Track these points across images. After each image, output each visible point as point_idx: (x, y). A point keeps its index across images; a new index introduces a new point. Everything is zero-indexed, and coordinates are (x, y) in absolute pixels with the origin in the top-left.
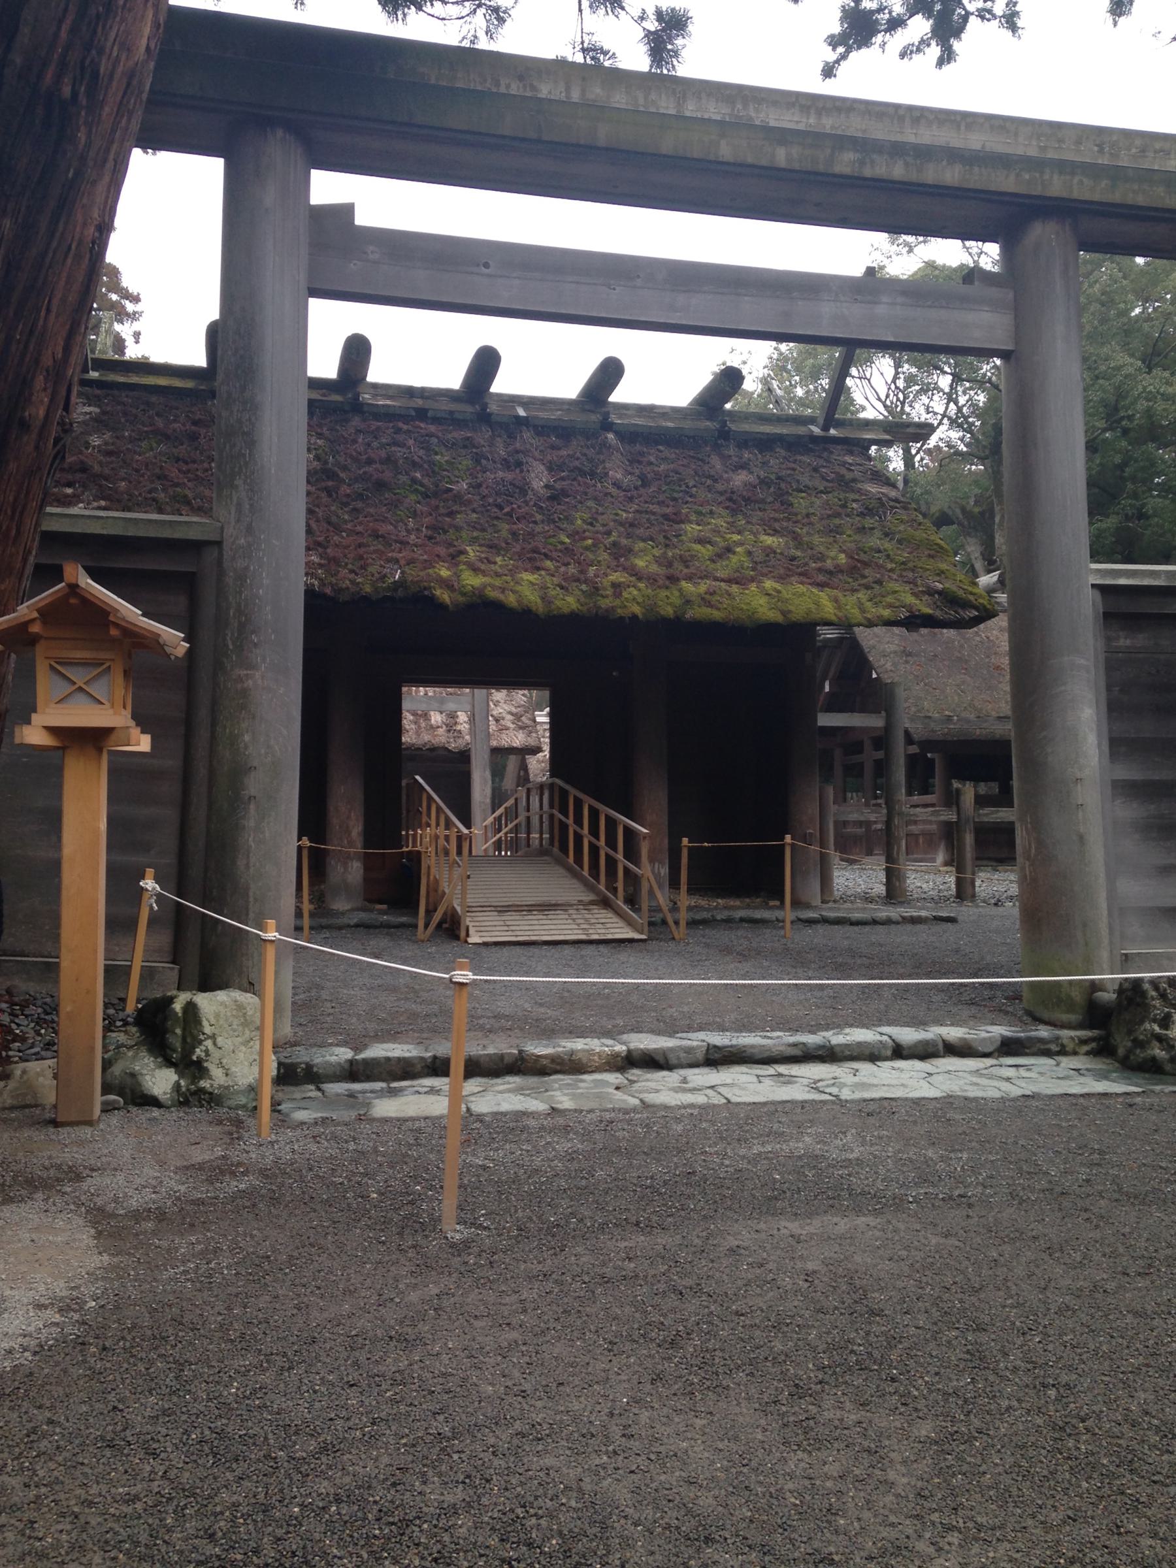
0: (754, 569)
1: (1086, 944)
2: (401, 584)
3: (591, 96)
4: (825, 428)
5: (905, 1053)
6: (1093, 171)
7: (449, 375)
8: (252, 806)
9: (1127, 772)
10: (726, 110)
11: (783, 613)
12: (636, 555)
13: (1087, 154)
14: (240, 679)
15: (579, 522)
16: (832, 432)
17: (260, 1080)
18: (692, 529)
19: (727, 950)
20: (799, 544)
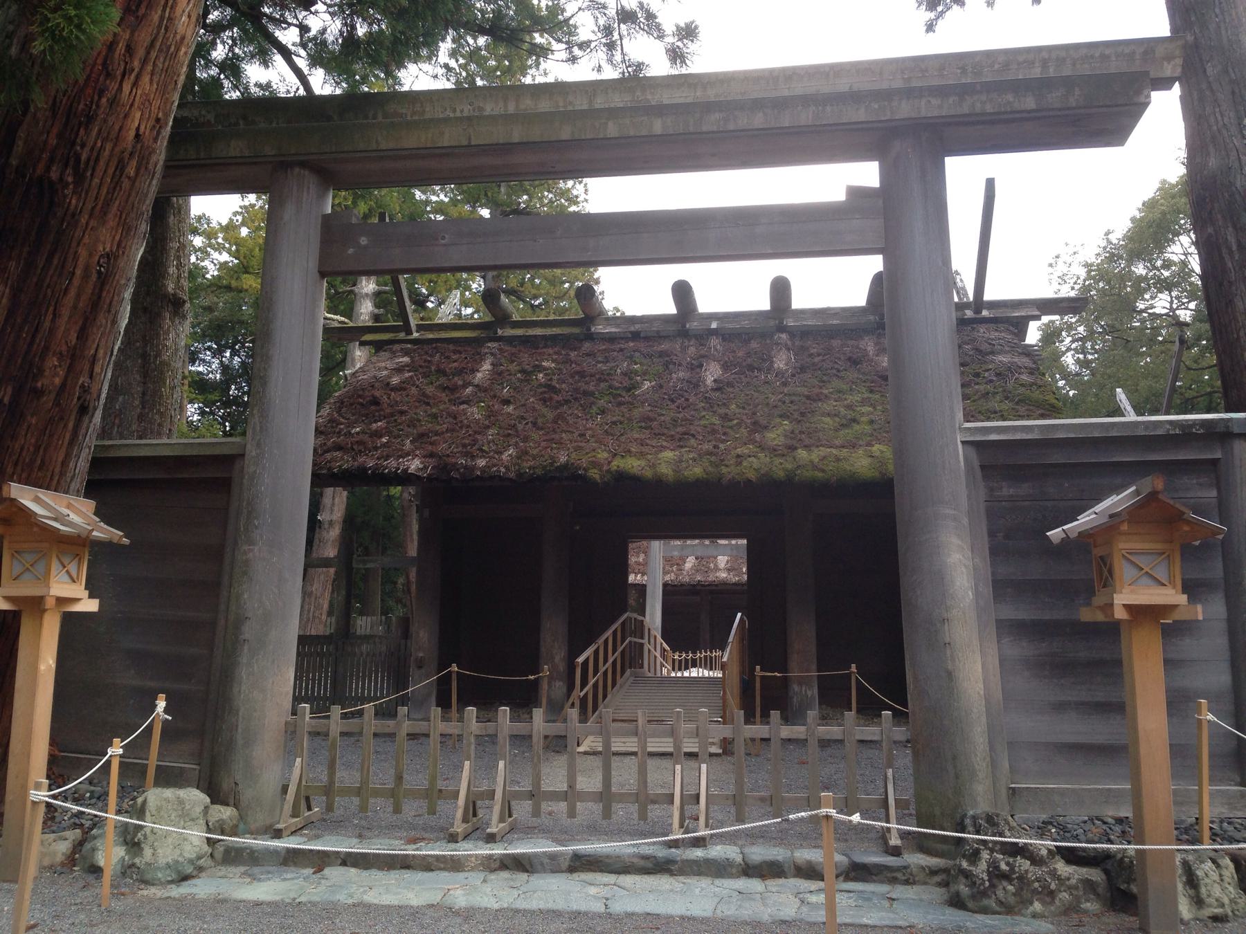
1: (957, 777)
2: (565, 467)
3: (522, 107)
5: (750, 872)
6: (941, 92)
7: (761, 302)
8: (246, 647)
9: (1010, 612)
10: (627, 97)
13: (865, 84)
14: (245, 553)
15: (733, 406)
16: (985, 313)
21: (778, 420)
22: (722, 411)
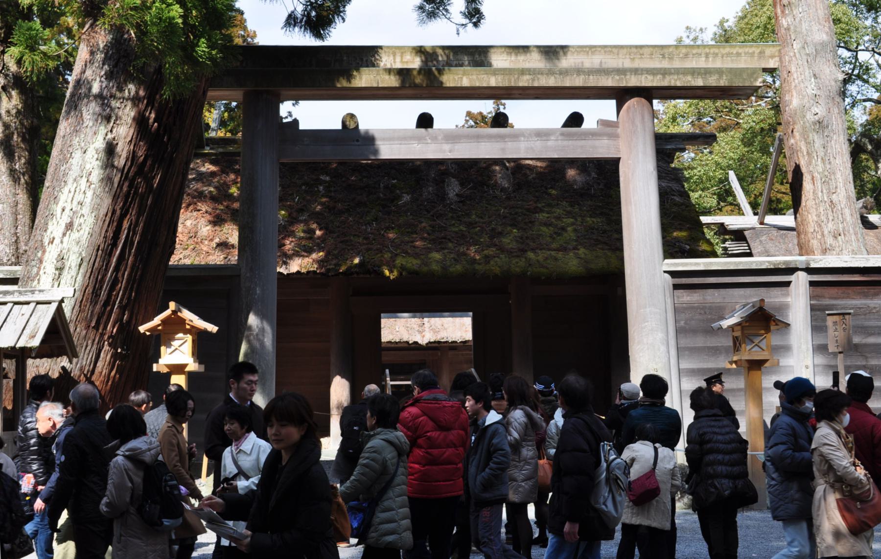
0: (576, 241)
15: (474, 217)
18: (542, 216)
19: (818, 515)
21: (509, 228)
22: (466, 219)
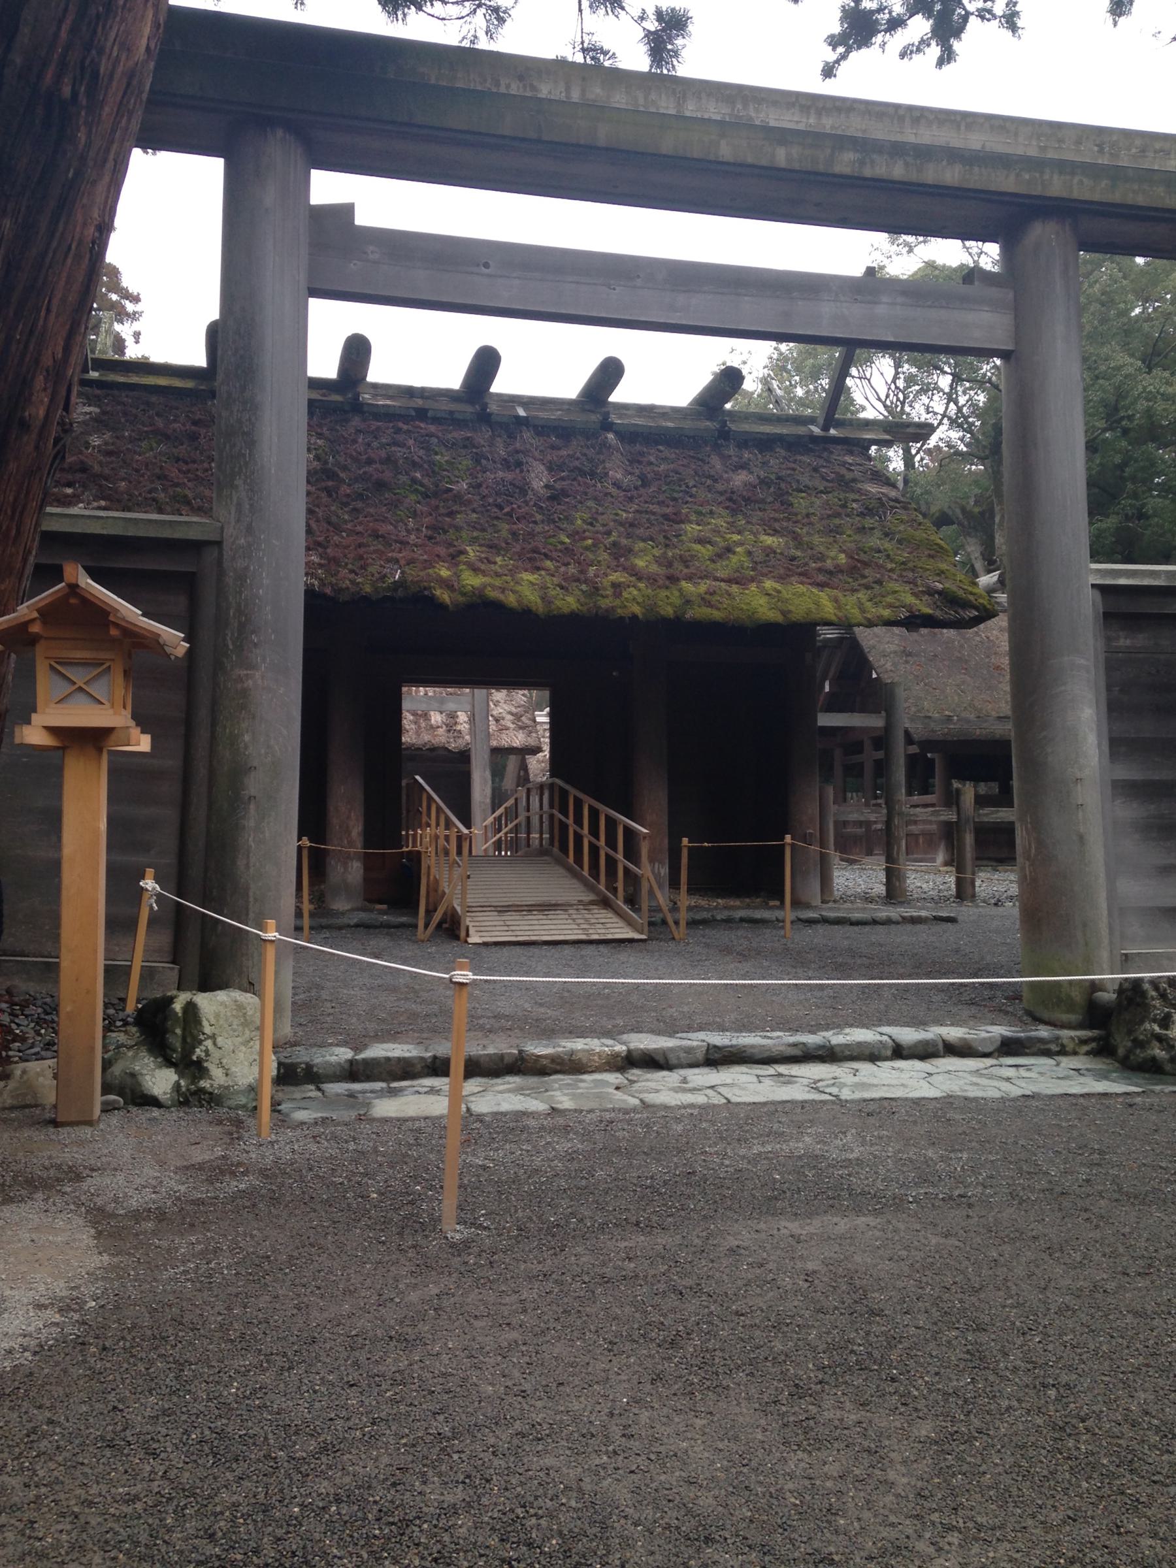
0: (754, 569)
1: (1086, 944)
2: (401, 584)
3: (591, 96)
4: (825, 428)
5: (905, 1053)
6: (1093, 171)
7: (449, 375)
8: (252, 806)
9: (1127, 772)
10: (726, 110)
11: (783, 613)
12: (636, 555)
13: (1087, 154)
14: (240, 679)
15: (579, 522)
16: (832, 432)
17: (260, 1080)
18: (692, 529)
19: (727, 950)
20: (799, 544)
